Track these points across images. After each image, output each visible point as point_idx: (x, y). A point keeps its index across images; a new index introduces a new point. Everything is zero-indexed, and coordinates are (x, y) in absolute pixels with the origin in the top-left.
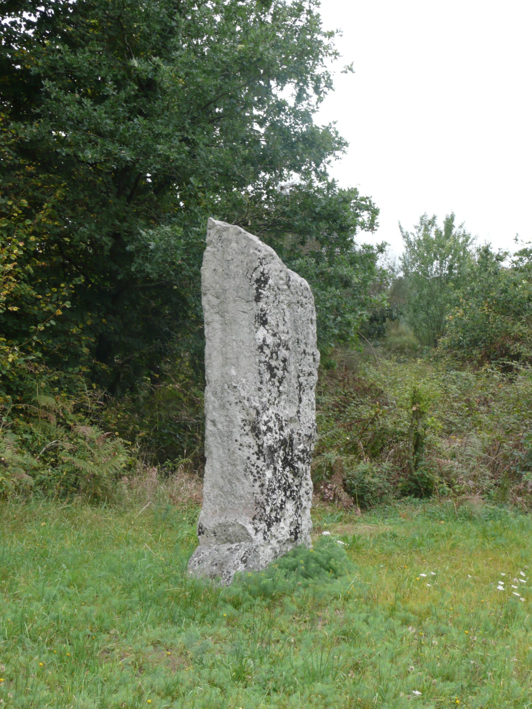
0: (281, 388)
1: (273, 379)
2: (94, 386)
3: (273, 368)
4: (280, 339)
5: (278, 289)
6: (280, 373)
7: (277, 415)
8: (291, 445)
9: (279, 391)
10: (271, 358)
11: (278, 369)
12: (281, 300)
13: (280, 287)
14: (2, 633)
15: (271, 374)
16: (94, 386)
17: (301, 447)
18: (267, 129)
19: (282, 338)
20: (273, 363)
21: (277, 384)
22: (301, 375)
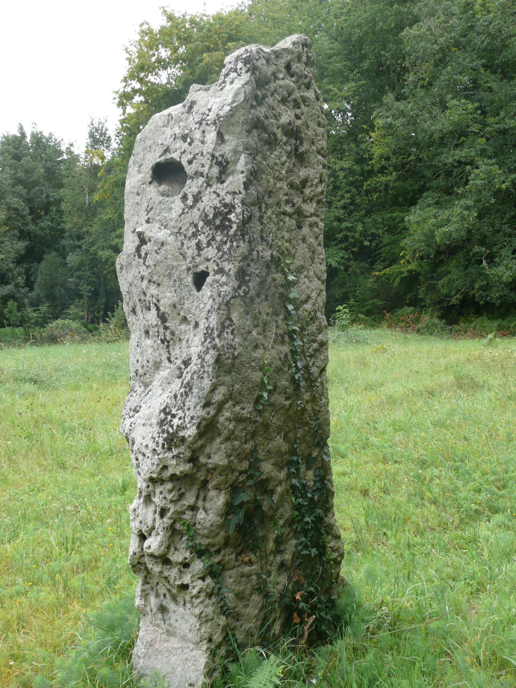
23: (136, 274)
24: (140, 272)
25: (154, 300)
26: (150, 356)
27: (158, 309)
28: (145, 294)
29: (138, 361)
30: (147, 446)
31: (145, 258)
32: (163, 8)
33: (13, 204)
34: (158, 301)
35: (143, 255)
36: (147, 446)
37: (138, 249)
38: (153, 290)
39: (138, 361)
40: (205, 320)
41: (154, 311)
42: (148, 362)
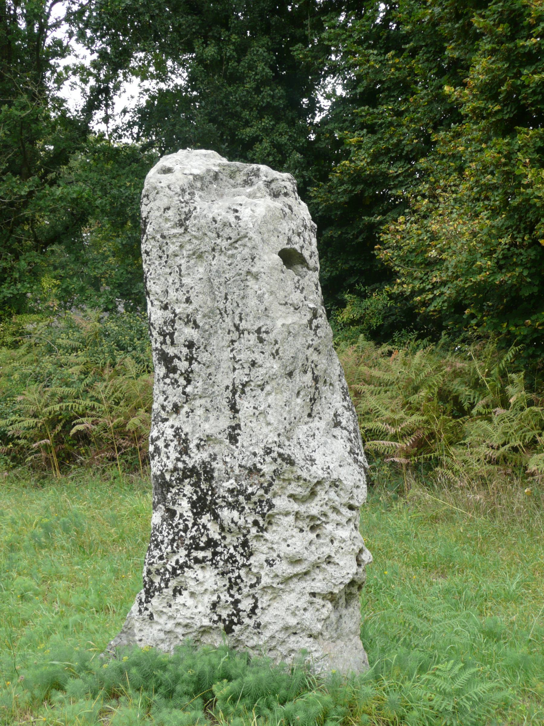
0: (189, 389)
1: (171, 375)
2: (151, 448)
3: (172, 358)
4: (174, 312)
5: (163, 237)
6: (183, 365)
7: (177, 432)
8: (210, 478)
9: (184, 393)
10: (164, 342)
11: (179, 359)
12: (170, 252)
13: (166, 233)
14: (212, 724)
15: (167, 367)
16: (151, 448)
17: (231, 484)
18: (334, 103)
19: (177, 311)
20: (171, 351)
21: (182, 381)
22: (237, 366)
23: (303, 342)
24: (307, 341)
25: (313, 365)
26: (297, 413)
27: (313, 373)
28: (307, 359)
29: (285, 419)
30: (359, 480)
31: (315, 330)
32: (230, 208)
33: (370, 85)
34: (316, 366)
35: (313, 328)
36: (359, 480)
37: (310, 322)
38: (315, 357)
39: (285, 419)
40: (338, 383)
41: (309, 374)
42: (295, 418)
